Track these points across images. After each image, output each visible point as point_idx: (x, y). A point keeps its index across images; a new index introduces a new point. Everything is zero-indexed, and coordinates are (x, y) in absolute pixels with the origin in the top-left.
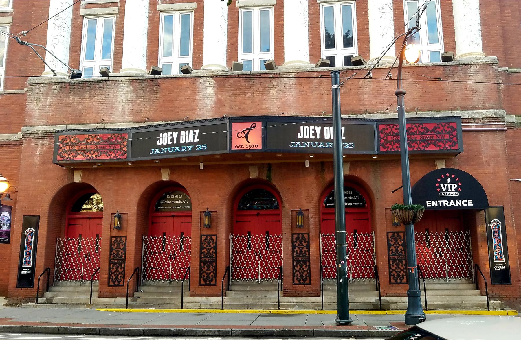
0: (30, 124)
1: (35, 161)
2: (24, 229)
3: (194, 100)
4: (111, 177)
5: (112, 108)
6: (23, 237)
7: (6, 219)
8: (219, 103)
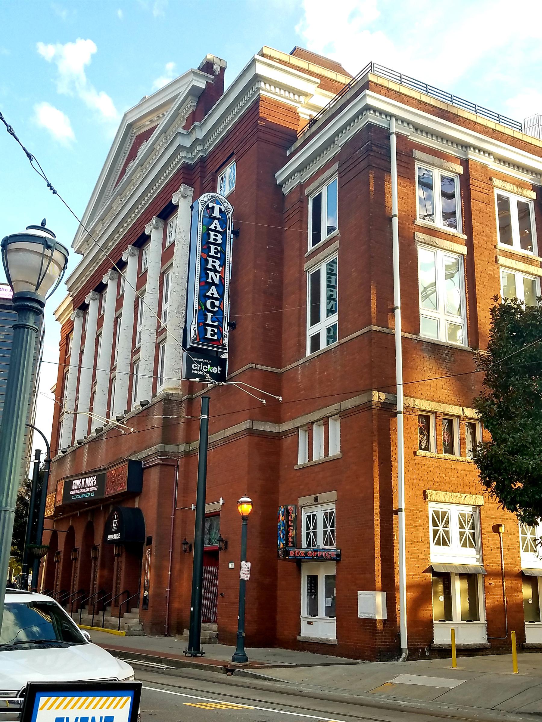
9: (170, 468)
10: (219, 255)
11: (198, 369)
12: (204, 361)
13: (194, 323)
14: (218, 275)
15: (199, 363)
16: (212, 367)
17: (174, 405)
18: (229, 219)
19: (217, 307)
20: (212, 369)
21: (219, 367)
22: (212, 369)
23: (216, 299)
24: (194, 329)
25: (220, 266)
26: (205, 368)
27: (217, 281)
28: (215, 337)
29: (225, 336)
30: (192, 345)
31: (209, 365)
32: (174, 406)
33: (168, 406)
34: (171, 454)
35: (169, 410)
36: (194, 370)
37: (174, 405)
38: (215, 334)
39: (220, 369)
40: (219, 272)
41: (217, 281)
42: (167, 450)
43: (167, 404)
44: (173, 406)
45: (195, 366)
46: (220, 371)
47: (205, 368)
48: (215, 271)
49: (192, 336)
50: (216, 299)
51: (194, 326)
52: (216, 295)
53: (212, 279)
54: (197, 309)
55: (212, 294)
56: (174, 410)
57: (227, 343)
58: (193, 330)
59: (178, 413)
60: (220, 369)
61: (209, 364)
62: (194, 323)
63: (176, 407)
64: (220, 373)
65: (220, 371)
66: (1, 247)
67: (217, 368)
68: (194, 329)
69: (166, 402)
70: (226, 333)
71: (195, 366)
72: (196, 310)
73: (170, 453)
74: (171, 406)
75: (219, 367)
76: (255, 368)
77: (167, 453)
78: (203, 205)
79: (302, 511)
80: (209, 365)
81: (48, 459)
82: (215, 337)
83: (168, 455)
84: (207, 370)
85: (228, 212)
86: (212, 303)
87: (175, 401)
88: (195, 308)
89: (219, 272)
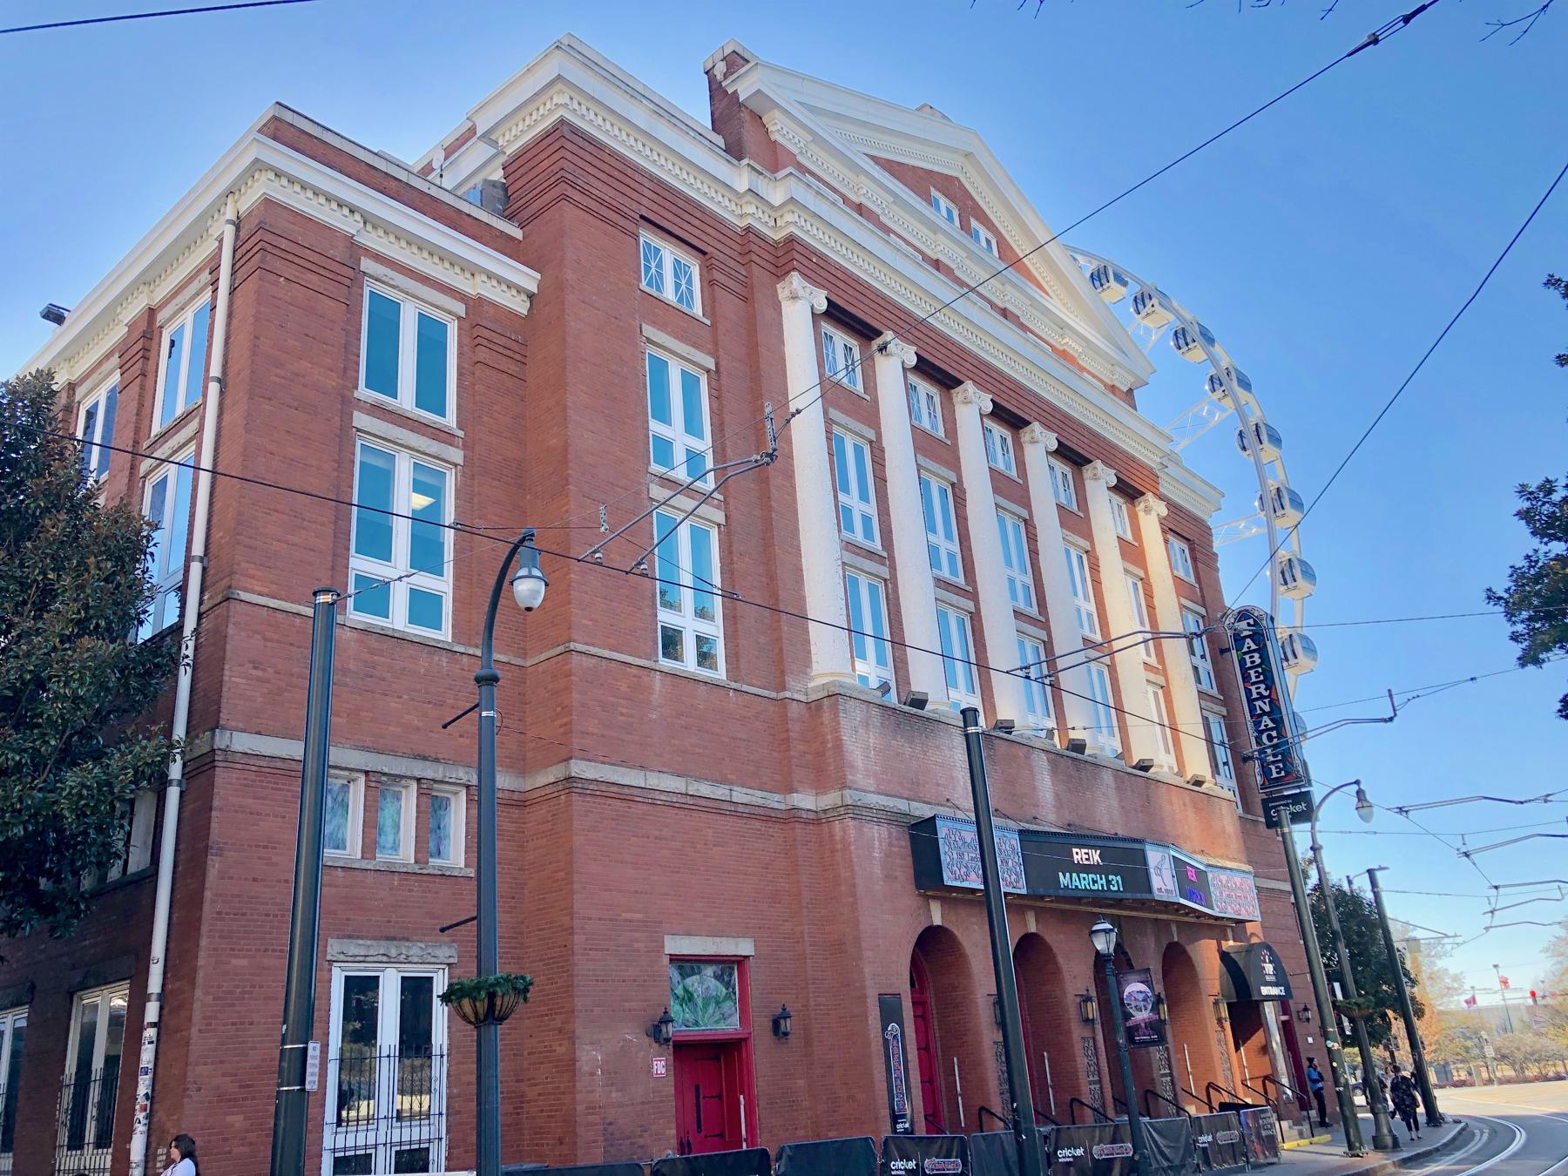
0: (855, 786)
1: (876, 871)
2: (884, 1029)
3: (1035, 788)
4: (974, 920)
5: (952, 778)
6: (886, 1042)
7: (1141, 997)
8: (1059, 803)
10: (1262, 678)
14: (1267, 701)
23: (1272, 729)
25: (1266, 689)
27: (1267, 709)
40: (1266, 697)
41: (1267, 709)
48: (1261, 697)
50: (1272, 729)
52: (1271, 725)
55: (1266, 726)
66: (1215, 550)
86: (1270, 738)
89: (1266, 697)
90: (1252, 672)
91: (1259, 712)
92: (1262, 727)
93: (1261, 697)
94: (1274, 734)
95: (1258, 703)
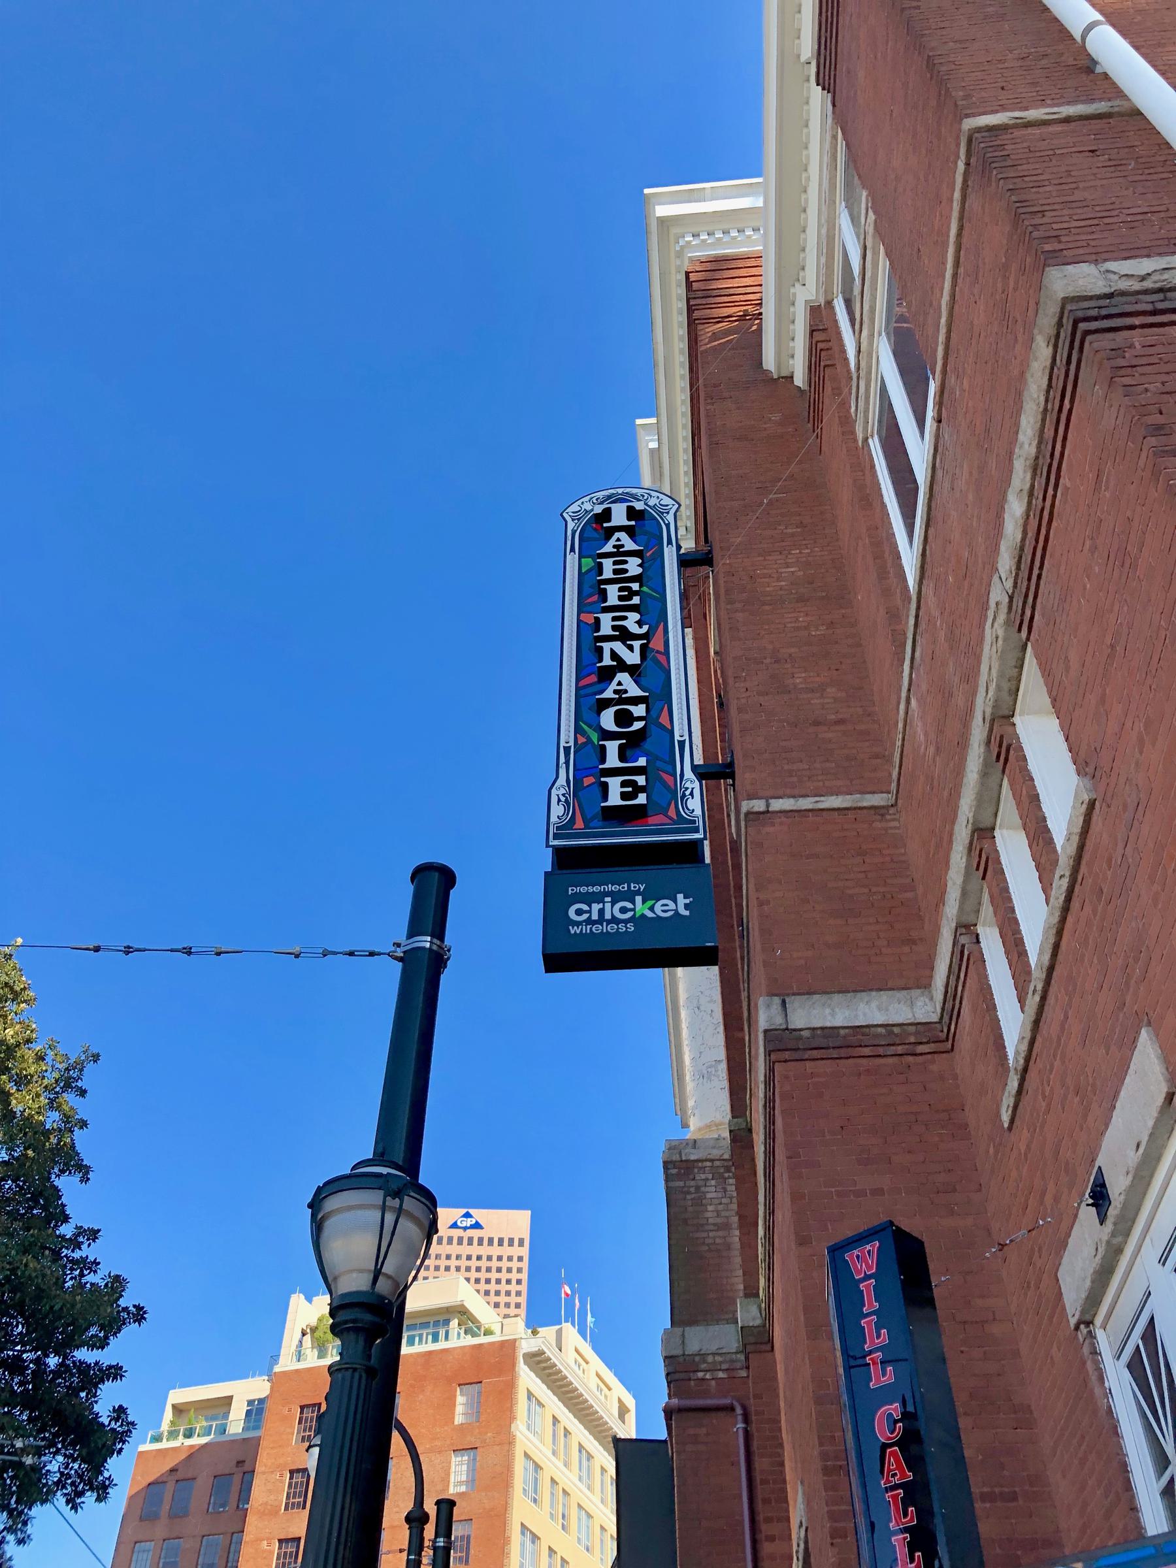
9: (715, 1419)
10: (636, 600)
11: (595, 917)
12: (615, 888)
13: (562, 780)
14: (637, 644)
15: (589, 899)
16: (649, 903)
17: (703, 1176)
18: (668, 526)
19: (640, 719)
20: (652, 909)
21: (680, 897)
22: (652, 909)
23: (635, 701)
24: (563, 799)
26: (623, 910)
27: (633, 658)
28: (642, 799)
29: (688, 793)
30: (556, 843)
31: (639, 899)
32: (707, 1179)
33: (681, 1184)
34: (714, 1362)
35: (688, 1197)
36: (578, 924)
37: (703, 1176)
38: (638, 789)
39: (687, 901)
42: (693, 1347)
43: (679, 1177)
44: (701, 1183)
45: (579, 912)
46: (686, 906)
47: (623, 910)
49: (554, 819)
50: (635, 701)
51: (563, 791)
53: (614, 655)
54: (572, 744)
56: (709, 1196)
57: (698, 812)
58: (559, 800)
59: (724, 1201)
60: (687, 901)
61: (638, 893)
62: (562, 780)
63: (713, 1183)
64: (687, 913)
65: (686, 906)
67: (675, 901)
68: (563, 799)
69: (674, 1171)
70: (688, 785)
71: (579, 912)
72: (567, 750)
73: (710, 1359)
74: (692, 1183)
75: (680, 897)
76: (768, 812)
77: (697, 1359)
78: (578, 519)
79: (1095, 1352)
80: (639, 899)
81: (416, 1515)
82: (642, 799)
83: (703, 1366)
84: (630, 914)
85: (662, 513)
87: (708, 1164)
88: (562, 744)
90: (614, 783)
91: (607, 661)
92: (609, 694)
93: (624, 635)
94: (639, 710)
95: (607, 646)
